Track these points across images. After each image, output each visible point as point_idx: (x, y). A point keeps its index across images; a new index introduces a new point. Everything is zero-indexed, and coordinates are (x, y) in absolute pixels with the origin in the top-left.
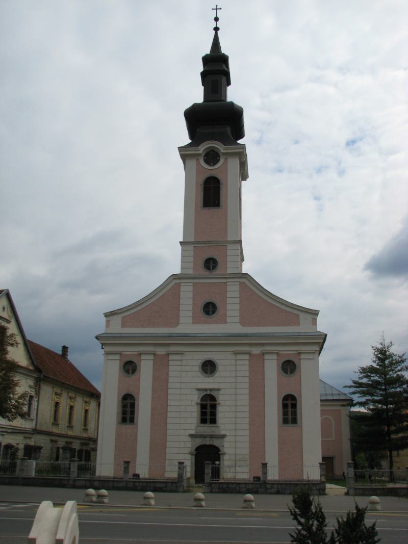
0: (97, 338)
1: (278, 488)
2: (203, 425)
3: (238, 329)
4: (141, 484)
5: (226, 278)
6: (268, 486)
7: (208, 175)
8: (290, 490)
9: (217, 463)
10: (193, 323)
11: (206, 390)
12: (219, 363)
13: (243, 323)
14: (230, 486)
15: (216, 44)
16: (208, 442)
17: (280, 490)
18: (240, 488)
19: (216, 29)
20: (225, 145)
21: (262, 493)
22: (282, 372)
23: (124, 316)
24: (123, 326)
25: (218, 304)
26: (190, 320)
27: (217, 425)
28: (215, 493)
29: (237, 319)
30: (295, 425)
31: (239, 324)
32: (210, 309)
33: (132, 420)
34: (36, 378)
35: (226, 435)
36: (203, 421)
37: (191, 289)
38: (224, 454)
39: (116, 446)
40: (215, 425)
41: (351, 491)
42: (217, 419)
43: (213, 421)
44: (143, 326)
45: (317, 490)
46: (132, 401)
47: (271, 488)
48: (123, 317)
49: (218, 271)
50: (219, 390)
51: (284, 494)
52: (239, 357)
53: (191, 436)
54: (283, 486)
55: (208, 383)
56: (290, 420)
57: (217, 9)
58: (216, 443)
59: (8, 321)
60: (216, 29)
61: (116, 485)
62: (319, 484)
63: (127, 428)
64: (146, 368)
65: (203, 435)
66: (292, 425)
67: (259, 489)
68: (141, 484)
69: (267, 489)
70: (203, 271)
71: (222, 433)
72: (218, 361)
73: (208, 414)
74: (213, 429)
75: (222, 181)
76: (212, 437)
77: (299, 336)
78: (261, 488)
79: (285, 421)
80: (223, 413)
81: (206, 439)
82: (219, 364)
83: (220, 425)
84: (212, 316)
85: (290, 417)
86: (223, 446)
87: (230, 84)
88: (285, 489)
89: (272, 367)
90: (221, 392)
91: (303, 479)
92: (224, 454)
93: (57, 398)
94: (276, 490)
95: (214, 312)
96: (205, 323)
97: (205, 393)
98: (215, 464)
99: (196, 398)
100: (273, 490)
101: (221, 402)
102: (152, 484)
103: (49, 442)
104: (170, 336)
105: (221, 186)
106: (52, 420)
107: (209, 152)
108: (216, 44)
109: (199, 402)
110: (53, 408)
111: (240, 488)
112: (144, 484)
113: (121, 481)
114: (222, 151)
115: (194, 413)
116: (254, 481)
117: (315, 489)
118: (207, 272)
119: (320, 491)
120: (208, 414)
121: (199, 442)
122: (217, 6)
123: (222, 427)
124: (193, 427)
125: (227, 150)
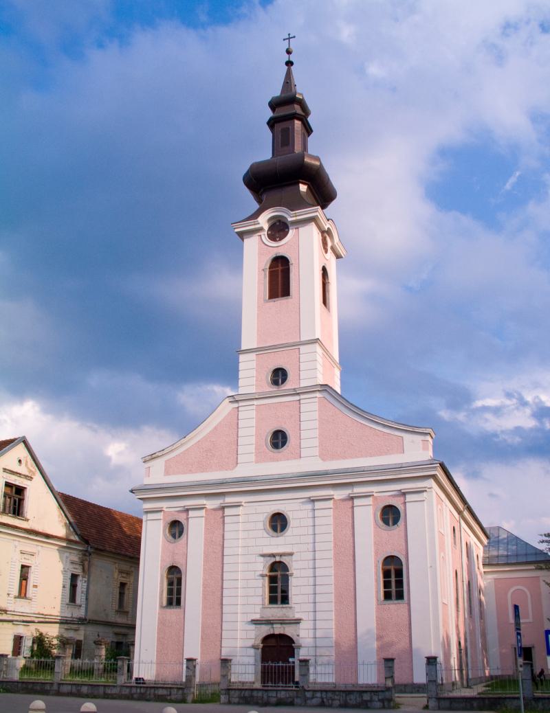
0: (132, 491)
1: (322, 698)
2: (271, 606)
3: (319, 465)
4: (138, 690)
5: (298, 394)
6: (308, 695)
7: (273, 254)
8: (339, 700)
9: (291, 660)
10: (257, 462)
11: (273, 555)
12: (290, 516)
13: (324, 456)
14: (255, 694)
15: (288, 82)
16: (278, 630)
17: (325, 700)
18: (268, 697)
19: (289, 63)
20: (292, 210)
21: (300, 706)
22: (381, 523)
23: (168, 460)
24: (167, 473)
25: (290, 433)
26: (253, 457)
27: (289, 606)
28: (234, 704)
29: (316, 451)
30: (400, 601)
31: (318, 457)
32: (279, 439)
33: (178, 603)
34: (81, 551)
35: (300, 620)
36: (273, 600)
37: (253, 414)
38: (299, 647)
39: (159, 639)
40: (287, 605)
41: (432, 703)
42: (290, 596)
43: (285, 599)
44: (191, 472)
45: (379, 700)
46: (178, 576)
47: (313, 698)
48: (166, 461)
49: (289, 385)
50: (291, 554)
51: (330, 706)
52: (318, 505)
53: (255, 622)
54: (330, 695)
55: (278, 544)
56: (394, 594)
57: (289, 39)
58: (288, 631)
59: (30, 478)
60: (289, 63)
61: (109, 691)
62: (382, 691)
63: (173, 612)
64: (196, 526)
65: (270, 620)
66: (396, 602)
67: (295, 700)
68: (138, 690)
69: (306, 699)
70: (270, 388)
71: (297, 616)
72: (288, 513)
73: (279, 590)
74: (284, 610)
75: (292, 261)
76: (282, 622)
77: (400, 468)
78: (297, 697)
79: (387, 596)
80: (298, 588)
81: (275, 626)
82: (291, 517)
83: (293, 606)
84: (281, 450)
85: (393, 589)
86: (298, 636)
87: (312, 131)
88: (333, 700)
89: (366, 515)
90: (294, 557)
91: (357, 684)
92: (299, 647)
93: (123, 577)
94: (319, 700)
95: (284, 444)
96: (273, 460)
97: (273, 560)
98: (289, 662)
99: (262, 567)
100: (315, 701)
101: (294, 572)
102: (152, 691)
103: (111, 635)
104: (222, 483)
105: (291, 266)
106: (116, 607)
107: (275, 223)
108: (288, 82)
109: (266, 572)
110: (117, 591)
111: (268, 697)
112: (142, 691)
113: (114, 686)
114: (290, 219)
115: (261, 588)
116: (263, 686)
117: (377, 699)
118: (274, 388)
119: (383, 703)
120: (279, 590)
121: (265, 630)
122: (289, 34)
123: (297, 608)
124: (258, 608)
125: (296, 216)
